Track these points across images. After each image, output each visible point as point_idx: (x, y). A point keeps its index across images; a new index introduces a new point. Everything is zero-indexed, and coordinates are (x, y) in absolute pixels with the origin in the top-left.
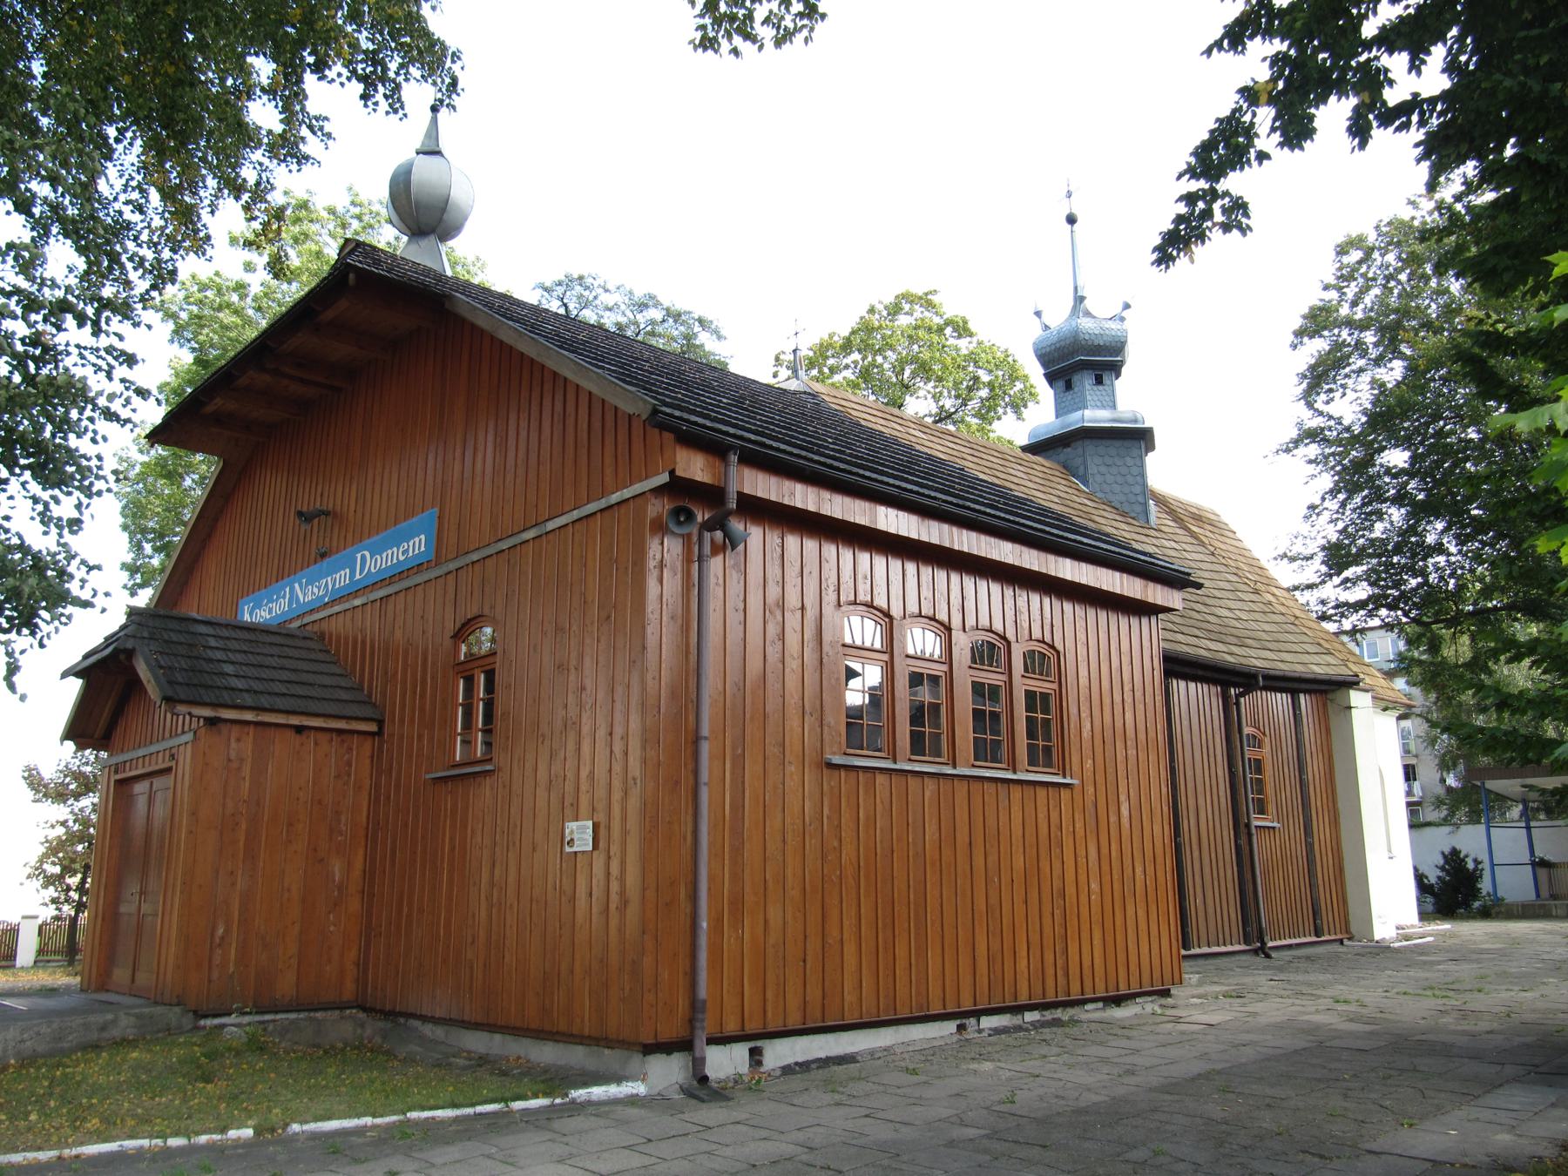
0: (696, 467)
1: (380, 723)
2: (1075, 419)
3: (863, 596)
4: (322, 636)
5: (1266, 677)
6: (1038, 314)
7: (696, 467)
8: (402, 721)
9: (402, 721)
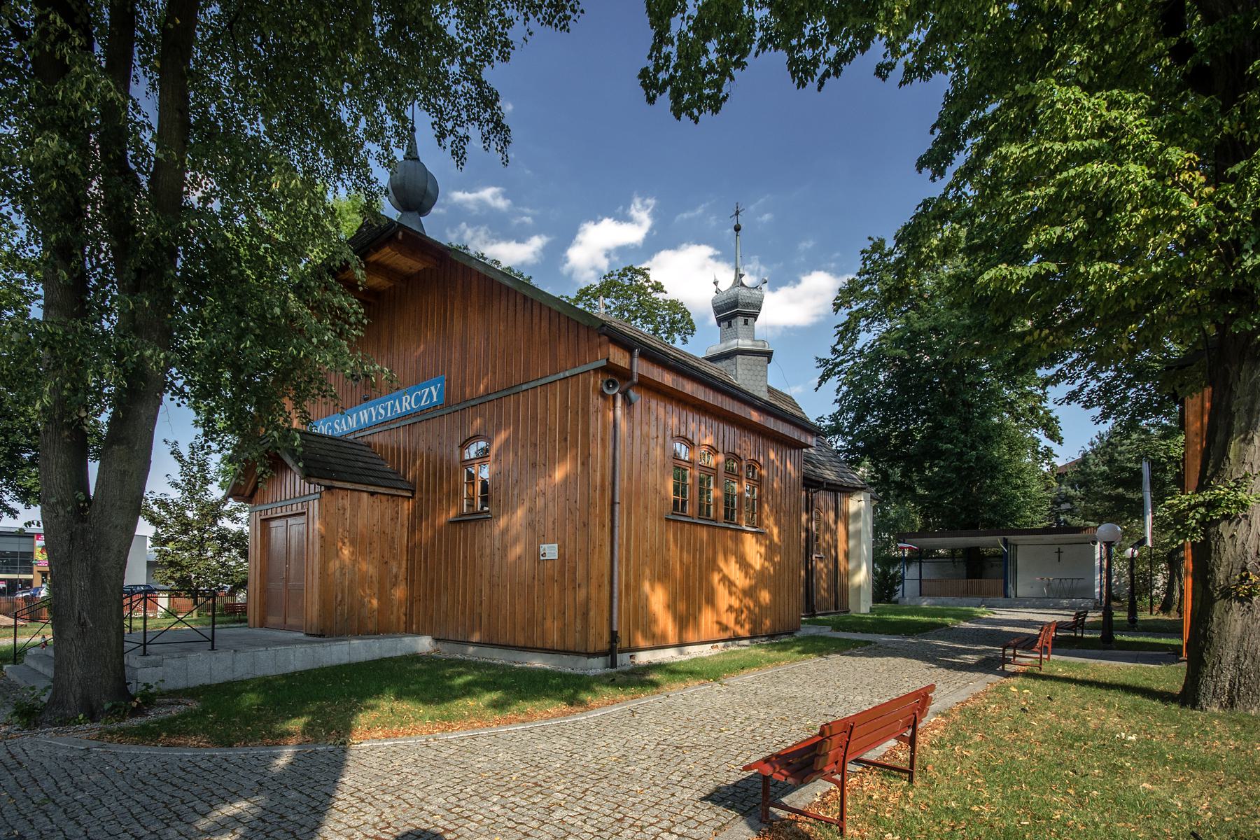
0: (619, 358)
1: (413, 492)
2: (734, 344)
3: (683, 433)
4: (369, 445)
5: (828, 484)
6: (716, 283)
7: (619, 358)
8: (428, 491)
9: (428, 491)
